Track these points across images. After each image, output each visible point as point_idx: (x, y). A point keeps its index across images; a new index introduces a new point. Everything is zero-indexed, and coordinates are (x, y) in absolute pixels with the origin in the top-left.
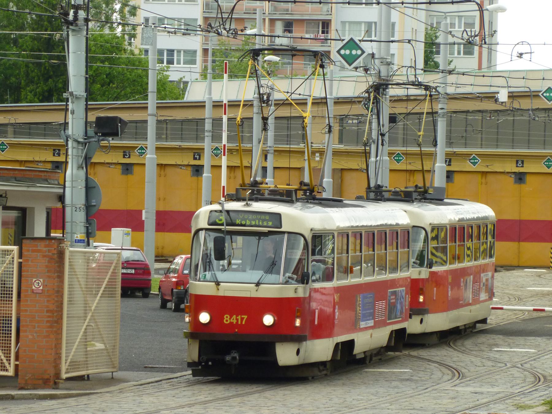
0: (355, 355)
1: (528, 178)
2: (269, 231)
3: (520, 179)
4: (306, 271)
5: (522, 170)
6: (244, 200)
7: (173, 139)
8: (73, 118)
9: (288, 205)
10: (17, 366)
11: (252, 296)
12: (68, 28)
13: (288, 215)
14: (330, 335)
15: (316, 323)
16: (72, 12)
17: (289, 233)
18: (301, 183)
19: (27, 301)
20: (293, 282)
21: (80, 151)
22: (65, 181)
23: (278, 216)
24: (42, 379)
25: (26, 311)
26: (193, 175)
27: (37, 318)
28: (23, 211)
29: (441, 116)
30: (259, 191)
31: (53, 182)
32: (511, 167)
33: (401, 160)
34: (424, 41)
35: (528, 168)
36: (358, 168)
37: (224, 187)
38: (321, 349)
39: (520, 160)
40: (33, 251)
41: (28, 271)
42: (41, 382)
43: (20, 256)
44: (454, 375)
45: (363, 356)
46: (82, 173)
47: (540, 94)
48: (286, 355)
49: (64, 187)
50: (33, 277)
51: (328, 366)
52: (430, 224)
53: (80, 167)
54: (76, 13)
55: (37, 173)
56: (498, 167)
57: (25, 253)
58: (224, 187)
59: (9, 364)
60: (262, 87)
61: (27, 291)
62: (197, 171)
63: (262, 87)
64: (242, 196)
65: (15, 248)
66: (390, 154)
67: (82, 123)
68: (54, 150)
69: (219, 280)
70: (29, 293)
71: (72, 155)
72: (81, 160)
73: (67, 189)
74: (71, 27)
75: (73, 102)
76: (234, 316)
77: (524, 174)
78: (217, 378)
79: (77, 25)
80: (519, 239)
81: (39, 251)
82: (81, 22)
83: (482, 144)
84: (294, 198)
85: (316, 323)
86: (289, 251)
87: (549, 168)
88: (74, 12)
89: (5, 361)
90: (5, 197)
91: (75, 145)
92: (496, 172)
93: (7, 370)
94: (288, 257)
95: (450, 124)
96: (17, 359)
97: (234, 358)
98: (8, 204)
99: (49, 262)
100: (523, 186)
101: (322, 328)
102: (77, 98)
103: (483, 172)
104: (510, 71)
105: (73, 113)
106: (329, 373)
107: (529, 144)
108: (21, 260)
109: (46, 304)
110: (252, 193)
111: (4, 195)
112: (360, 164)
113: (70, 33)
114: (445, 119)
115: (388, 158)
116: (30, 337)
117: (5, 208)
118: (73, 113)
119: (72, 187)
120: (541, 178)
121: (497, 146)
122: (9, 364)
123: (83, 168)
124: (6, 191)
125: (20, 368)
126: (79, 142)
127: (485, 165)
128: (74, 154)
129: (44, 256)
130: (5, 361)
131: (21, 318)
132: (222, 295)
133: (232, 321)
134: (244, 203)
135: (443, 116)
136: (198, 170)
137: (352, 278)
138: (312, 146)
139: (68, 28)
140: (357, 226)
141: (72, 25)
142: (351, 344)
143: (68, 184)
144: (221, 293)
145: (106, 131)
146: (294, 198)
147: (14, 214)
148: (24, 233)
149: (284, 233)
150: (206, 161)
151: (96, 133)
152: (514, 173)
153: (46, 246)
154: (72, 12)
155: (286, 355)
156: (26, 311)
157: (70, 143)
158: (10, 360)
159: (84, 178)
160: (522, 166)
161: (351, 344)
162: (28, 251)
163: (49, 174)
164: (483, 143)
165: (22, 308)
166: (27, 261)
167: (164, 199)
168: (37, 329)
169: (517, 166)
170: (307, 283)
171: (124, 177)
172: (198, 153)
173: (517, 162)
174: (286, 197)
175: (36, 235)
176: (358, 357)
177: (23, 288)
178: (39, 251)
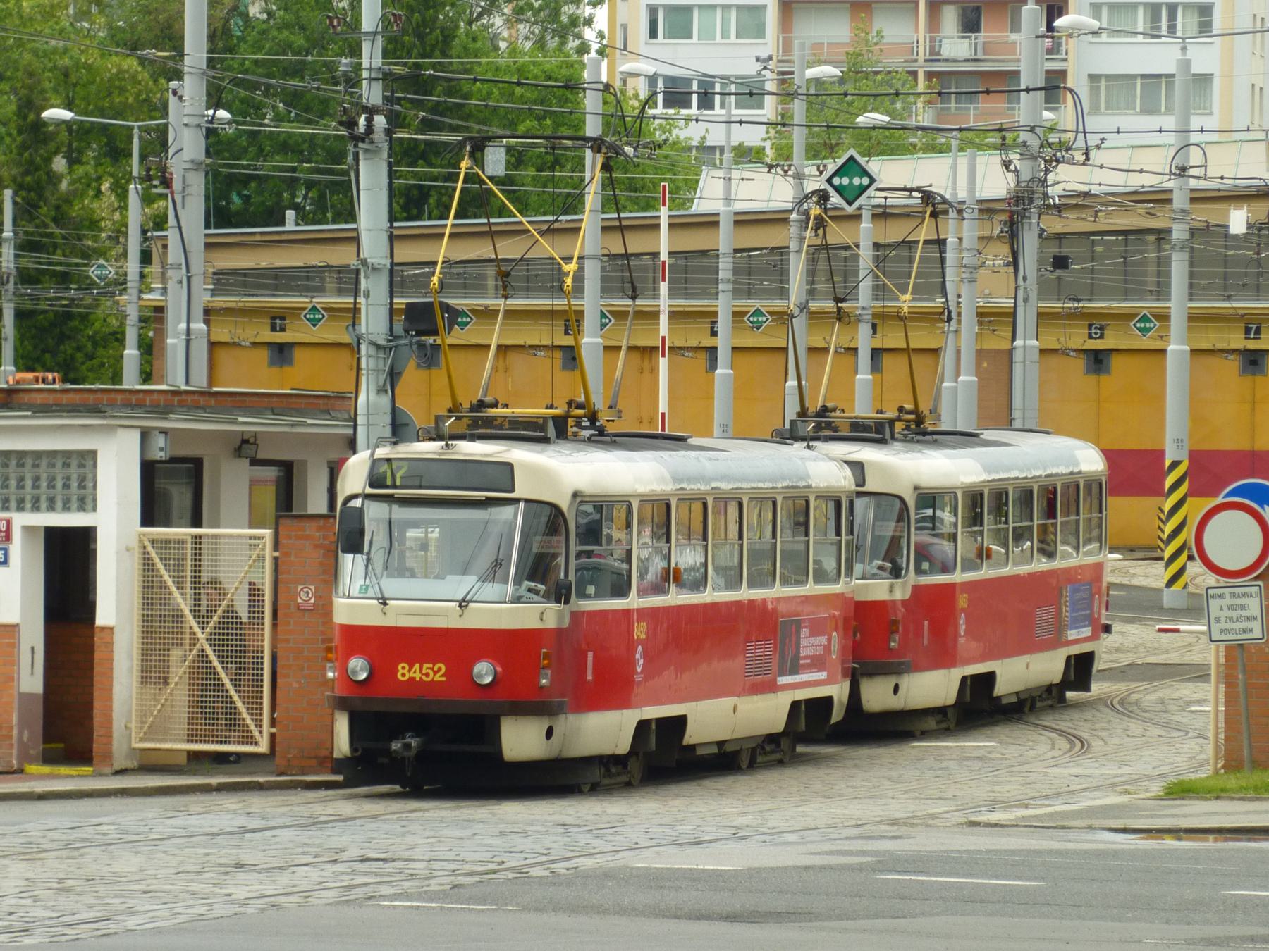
0: (999, 698)
2: (488, 499)
4: (562, 576)
6: (803, 439)
8: (367, 305)
9: (538, 447)
10: (273, 736)
11: (451, 626)
12: (356, 146)
13: (872, 464)
14: (623, 702)
15: (590, 677)
16: (362, 121)
17: (527, 501)
18: (901, 409)
19: (289, 623)
20: (536, 598)
21: (381, 362)
22: (356, 414)
23: (509, 467)
24: (316, 757)
25: (287, 641)
27: (306, 653)
28: (287, 469)
29: (1177, 248)
30: (829, 426)
31: (339, 416)
37: (663, 415)
38: (607, 730)
40: (298, 538)
41: (289, 572)
42: (314, 762)
43: (276, 546)
44: (1073, 745)
45: (1014, 699)
46: (385, 400)
48: (521, 740)
49: (355, 427)
50: (297, 582)
51: (950, 713)
52: (916, 488)
53: (381, 390)
54: (369, 120)
55: (311, 401)
57: (283, 541)
58: (663, 415)
59: (261, 732)
61: (288, 607)
64: (801, 434)
65: (267, 533)
67: (384, 312)
69: (386, 596)
70: (293, 610)
71: (368, 369)
72: (382, 378)
73: (359, 428)
74: (361, 145)
75: (367, 277)
76: (417, 666)
77: (291, 345)
78: (397, 788)
79: (372, 142)
81: (307, 538)
82: (379, 135)
84: (888, 436)
85: (590, 677)
86: (878, 523)
88: (367, 119)
89: (252, 727)
90: (255, 443)
91: (372, 351)
93: (256, 744)
94: (876, 533)
96: (273, 723)
97: (408, 746)
98: (260, 456)
99: (325, 555)
101: (610, 689)
102: (375, 269)
105: (367, 295)
106: (952, 726)
108: (277, 554)
109: (321, 628)
110: (818, 427)
111: (252, 440)
112: (1062, 339)
113: (361, 156)
115: (203, 326)
116: (295, 685)
117: (255, 462)
118: (367, 295)
119: (368, 425)
122: (261, 732)
123: (386, 391)
124: (255, 433)
125: (278, 739)
126: (378, 347)
128: (371, 366)
129: (316, 546)
130: (252, 727)
131: (279, 654)
132: (392, 624)
133: (412, 675)
134: (805, 444)
135: (1182, 249)
137: (990, 567)
139: (356, 146)
140: (1025, 478)
141: (363, 141)
142: (990, 678)
143: (360, 420)
144: (389, 621)
145: (423, 327)
146: (888, 436)
147: (271, 473)
148: (289, 507)
149: (517, 501)
151: (406, 331)
152: (269, 344)
153: (319, 529)
154: (362, 121)
155: (521, 740)
156: (287, 641)
157: (363, 348)
158: (261, 726)
159: (389, 410)
161: (990, 678)
162: (290, 538)
163: (332, 401)
165: (280, 636)
166: (287, 554)
168: (306, 671)
170: (567, 602)
174: (532, 432)
175: (311, 510)
176: (1004, 701)
177: (281, 602)
178: (307, 538)
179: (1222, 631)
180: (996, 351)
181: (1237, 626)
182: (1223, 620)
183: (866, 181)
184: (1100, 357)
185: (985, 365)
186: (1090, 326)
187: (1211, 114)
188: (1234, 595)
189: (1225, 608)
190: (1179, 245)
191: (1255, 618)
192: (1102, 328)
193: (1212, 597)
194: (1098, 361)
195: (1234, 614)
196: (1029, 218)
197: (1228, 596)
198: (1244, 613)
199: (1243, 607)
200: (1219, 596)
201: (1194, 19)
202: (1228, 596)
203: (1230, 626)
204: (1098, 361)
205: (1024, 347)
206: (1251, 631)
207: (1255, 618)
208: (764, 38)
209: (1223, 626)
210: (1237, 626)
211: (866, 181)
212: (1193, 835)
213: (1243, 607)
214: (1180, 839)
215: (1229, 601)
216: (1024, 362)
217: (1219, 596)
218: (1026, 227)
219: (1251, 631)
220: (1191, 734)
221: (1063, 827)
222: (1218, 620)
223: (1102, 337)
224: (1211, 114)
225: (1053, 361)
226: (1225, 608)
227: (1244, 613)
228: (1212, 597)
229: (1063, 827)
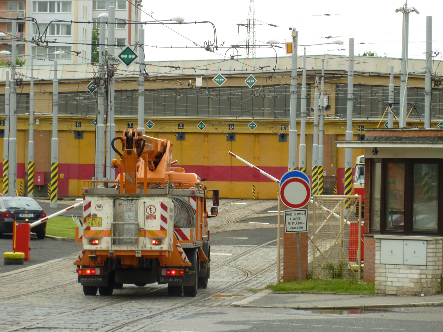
1: (187, 137)
3: (181, 137)
5: (183, 131)
7: (225, 114)
15: (4, 234)
26: (178, 139)
29: (140, 94)
32: (225, 130)
33: (152, 126)
34: (91, 43)
35: (187, 129)
36: (68, 130)
39: (181, 124)
47: (226, 79)
56: (167, 129)
60: (17, 74)
62: (181, 137)
63: (17, 74)
66: (117, 121)
68: (76, 123)
77: (184, 133)
80: (232, 180)
83: (154, 113)
85: (4, 234)
87: (201, 129)
92: (166, 133)
95: (146, 99)
100: (183, 142)
103: (155, 132)
104: (160, 62)
107: (187, 112)
112: (69, 127)
114: (143, 97)
120: (196, 136)
121: (165, 114)
127: (159, 127)
135: (142, 95)
136: (283, 137)
138: (324, 118)
150: (292, 130)
160: (183, 128)
164: (155, 112)
167: (258, 158)
169: (179, 128)
171: (280, 143)
172: (285, 125)
173: (179, 125)
179: (291, 228)
180: (45, 131)
181: (297, 226)
182: (291, 223)
183: (134, 56)
184: (80, 133)
185: (41, 135)
186: (76, 123)
187: (71, 59)
188: (295, 214)
189: (292, 219)
190: (141, 93)
191: (304, 223)
192: (80, 123)
193: (287, 215)
194: (79, 135)
195: (295, 221)
196: (112, 81)
197: (293, 214)
198: (299, 221)
199: (299, 219)
200: (290, 214)
201: (65, 30)
202: (293, 214)
203: (294, 226)
204: (79, 135)
205: (111, 126)
206: (302, 228)
207: (304, 223)
208: (39, 11)
209: (291, 226)
210: (297, 226)
211: (134, 56)
212: (315, 311)
213: (299, 219)
214: (341, 313)
215: (293, 216)
216: (110, 131)
217: (290, 214)
218: (111, 84)
219: (302, 228)
220: (220, 264)
221: (275, 308)
222: (289, 224)
223: (80, 126)
224: (71, 59)
225: (64, 134)
226: (292, 219)
227: (299, 221)
228: (287, 215)
229: (275, 308)
